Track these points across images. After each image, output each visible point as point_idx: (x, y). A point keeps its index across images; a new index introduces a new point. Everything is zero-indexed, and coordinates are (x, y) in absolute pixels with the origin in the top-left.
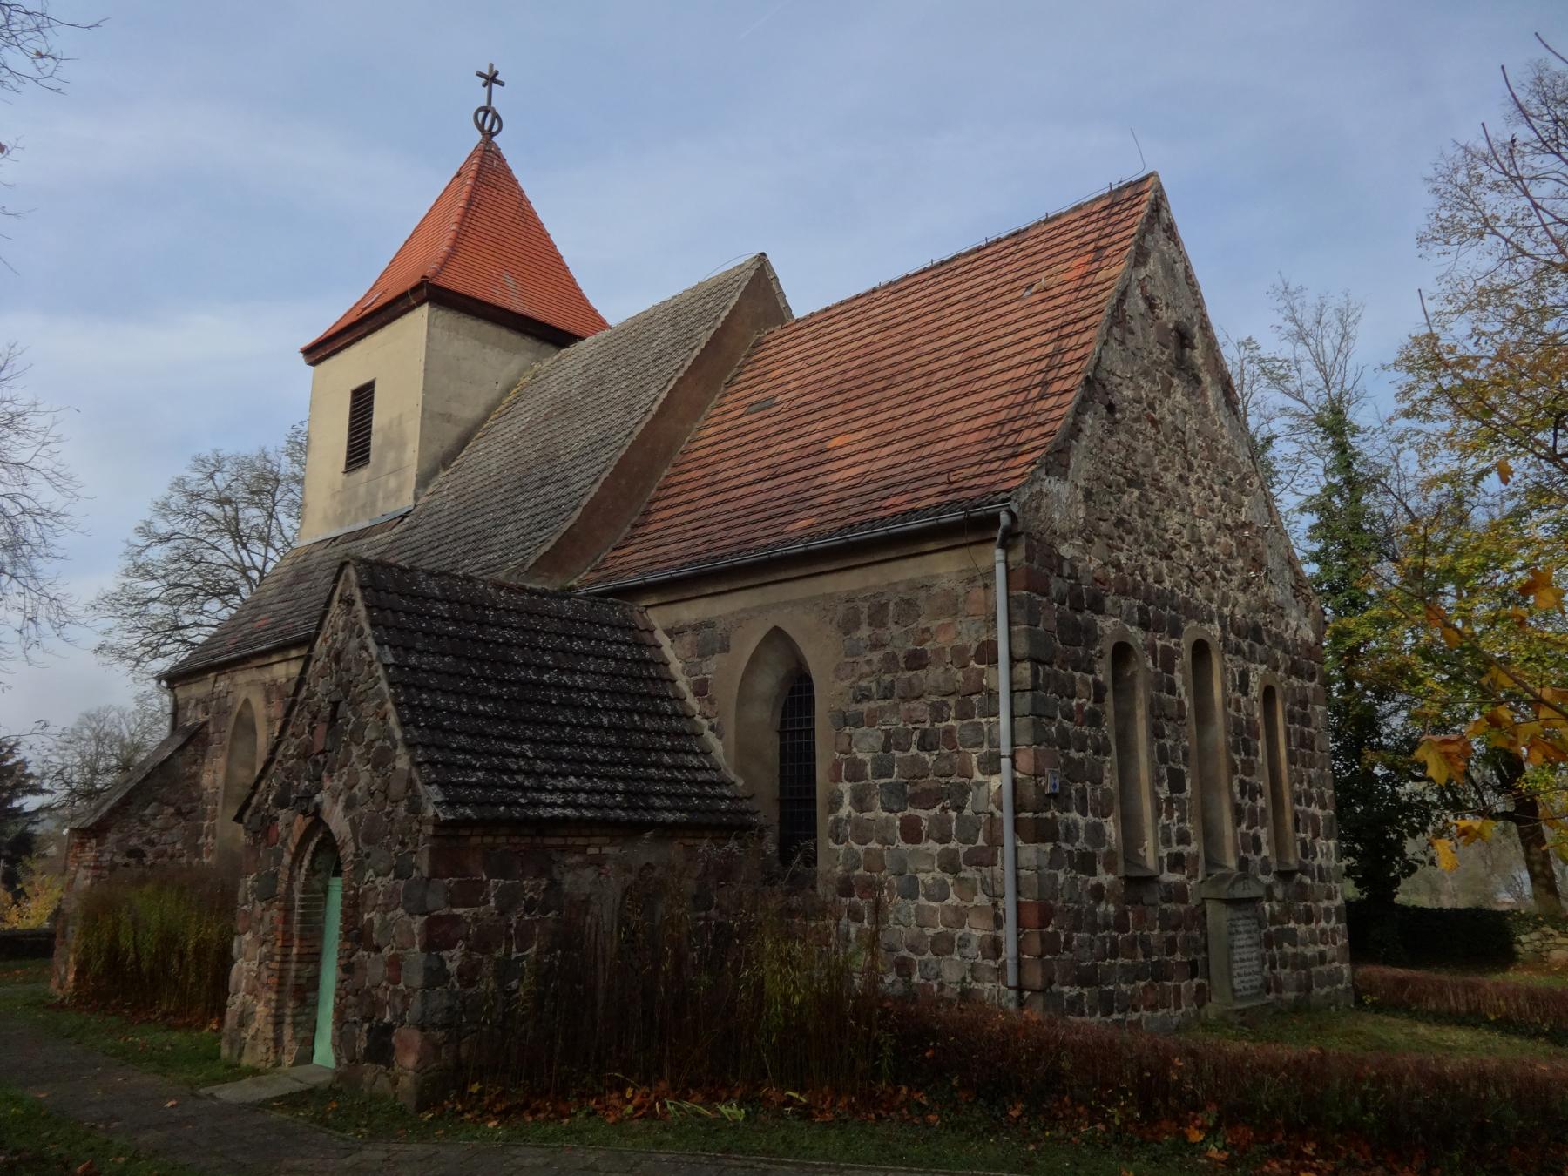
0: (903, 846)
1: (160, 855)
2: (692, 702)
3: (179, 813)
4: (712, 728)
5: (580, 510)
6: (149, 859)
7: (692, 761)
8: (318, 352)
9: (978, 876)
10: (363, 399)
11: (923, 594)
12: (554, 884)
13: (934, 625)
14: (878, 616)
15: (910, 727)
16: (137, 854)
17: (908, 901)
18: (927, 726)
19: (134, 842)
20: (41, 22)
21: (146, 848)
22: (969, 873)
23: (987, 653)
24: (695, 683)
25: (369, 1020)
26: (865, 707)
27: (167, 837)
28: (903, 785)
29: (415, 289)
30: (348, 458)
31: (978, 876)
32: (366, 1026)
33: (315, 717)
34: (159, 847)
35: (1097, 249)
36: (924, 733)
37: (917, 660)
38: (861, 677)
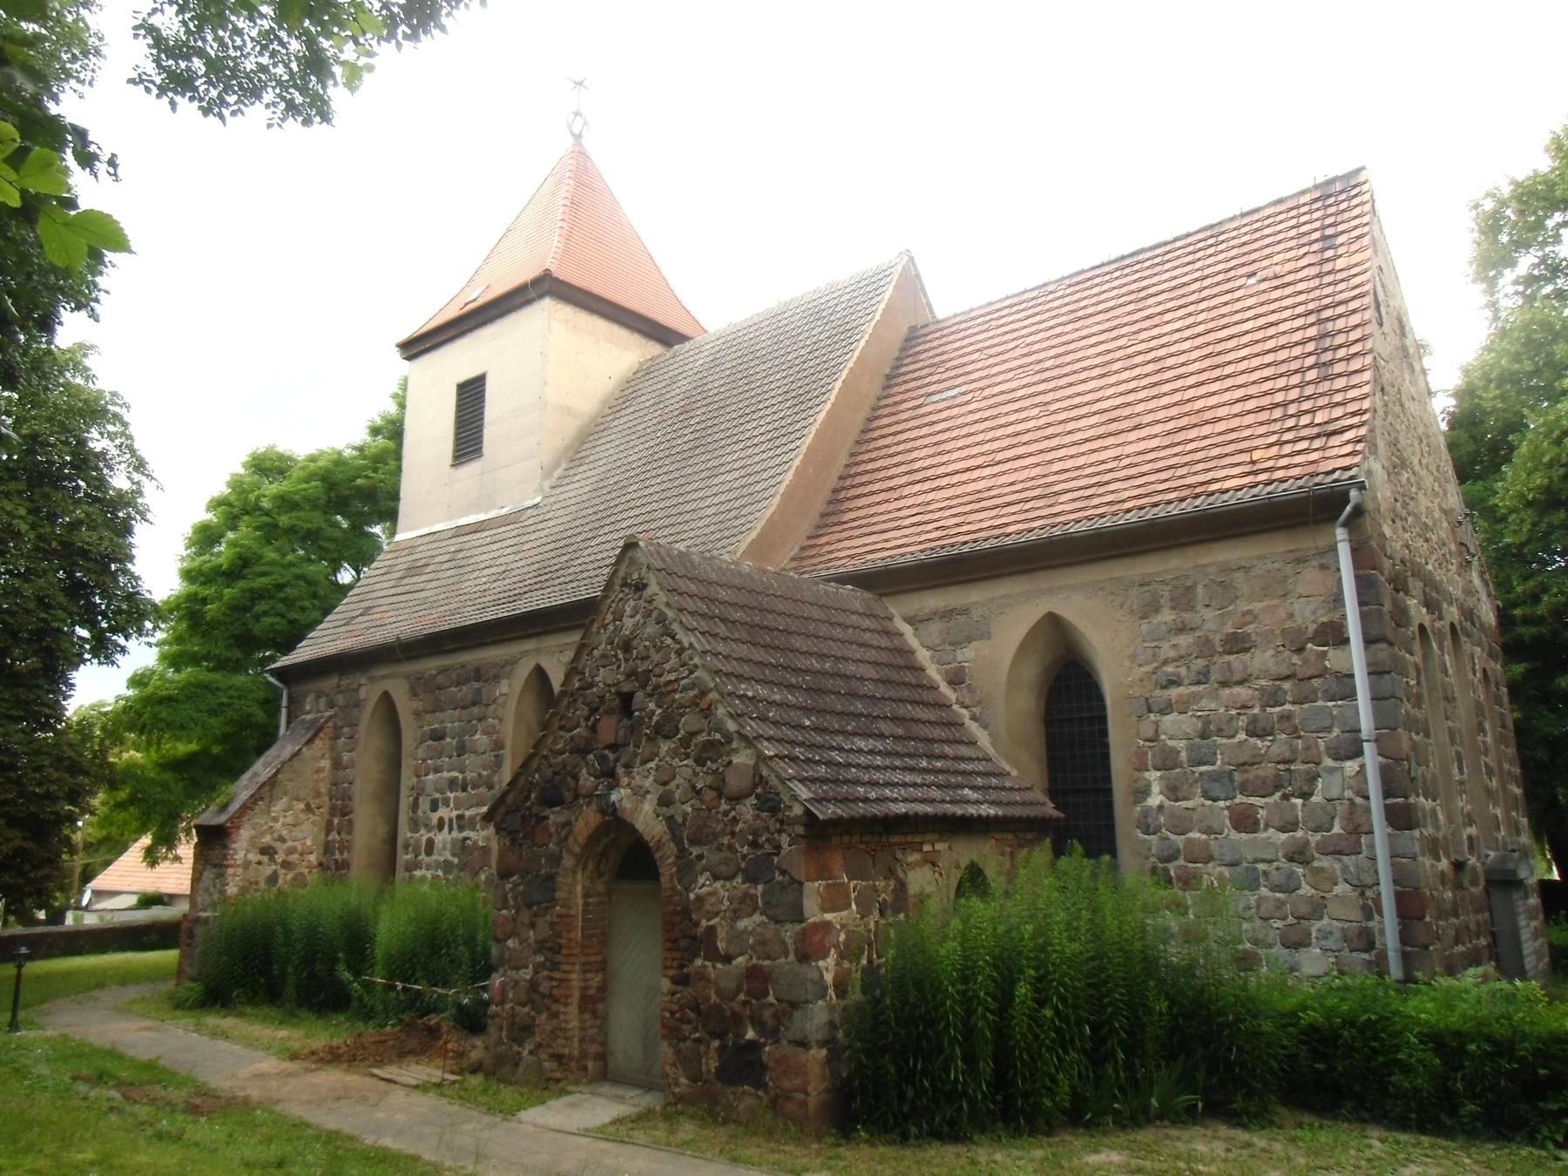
0: (1234, 835)
1: (292, 851)
2: (945, 689)
3: (308, 808)
4: (973, 718)
5: (778, 497)
6: (279, 858)
7: (964, 751)
8: (414, 348)
9: (1337, 866)
10: (471, 395)
11: (1239, 575)
12: (902, 886)
13: (1257, 606)
14: (1184, 599)
15: (1234, 712)
16: (268, 851)
17: (1246, 892)
18: (1256, 711)
19: (267, 839)
20: (337, 5)
21: (277, 845)
22: (1324, 862)
23: (1334, 635)
24: (947, 672)
25: (721, 1036)
26: (1174, 692)
27: (297, 833)
28: (1230, 774)
29: (537, 282)
30: (455, 451)
31: (1337, 866)
32: (716, 1043)
33: (594, 710)
34: (290, 843)
35: (1324, 238)
36: (1254, 720)
37: (1237, 644)
38: (1165, 662)
